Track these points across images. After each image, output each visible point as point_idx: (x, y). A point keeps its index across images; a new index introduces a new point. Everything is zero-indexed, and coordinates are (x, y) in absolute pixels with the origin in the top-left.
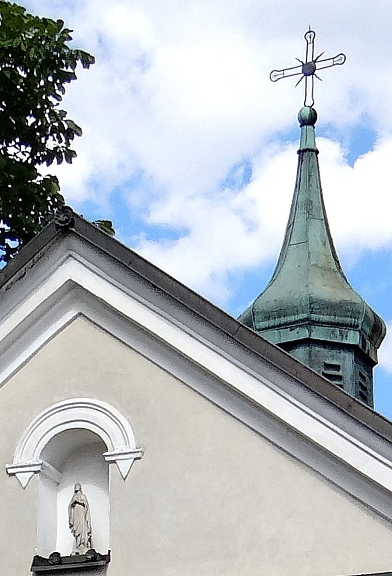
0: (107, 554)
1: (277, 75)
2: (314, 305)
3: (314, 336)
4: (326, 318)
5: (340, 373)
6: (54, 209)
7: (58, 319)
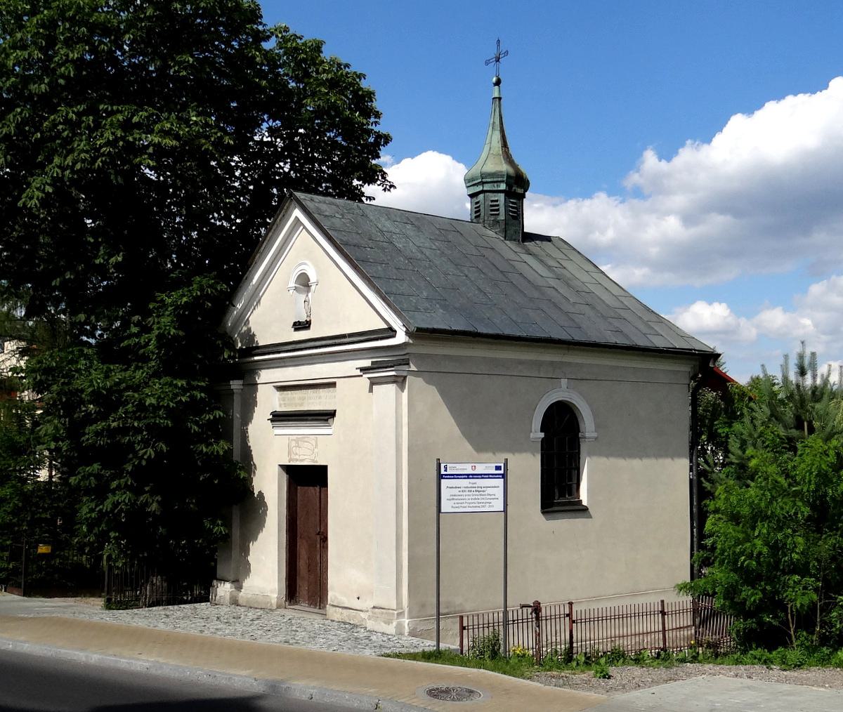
0: (375, 387)
1: (487, 63)
2: (483, 175)
3: (485, 189)
4: (489, 180)
5: (498, 203)
6: (283, 50)
7: (283, 229)
